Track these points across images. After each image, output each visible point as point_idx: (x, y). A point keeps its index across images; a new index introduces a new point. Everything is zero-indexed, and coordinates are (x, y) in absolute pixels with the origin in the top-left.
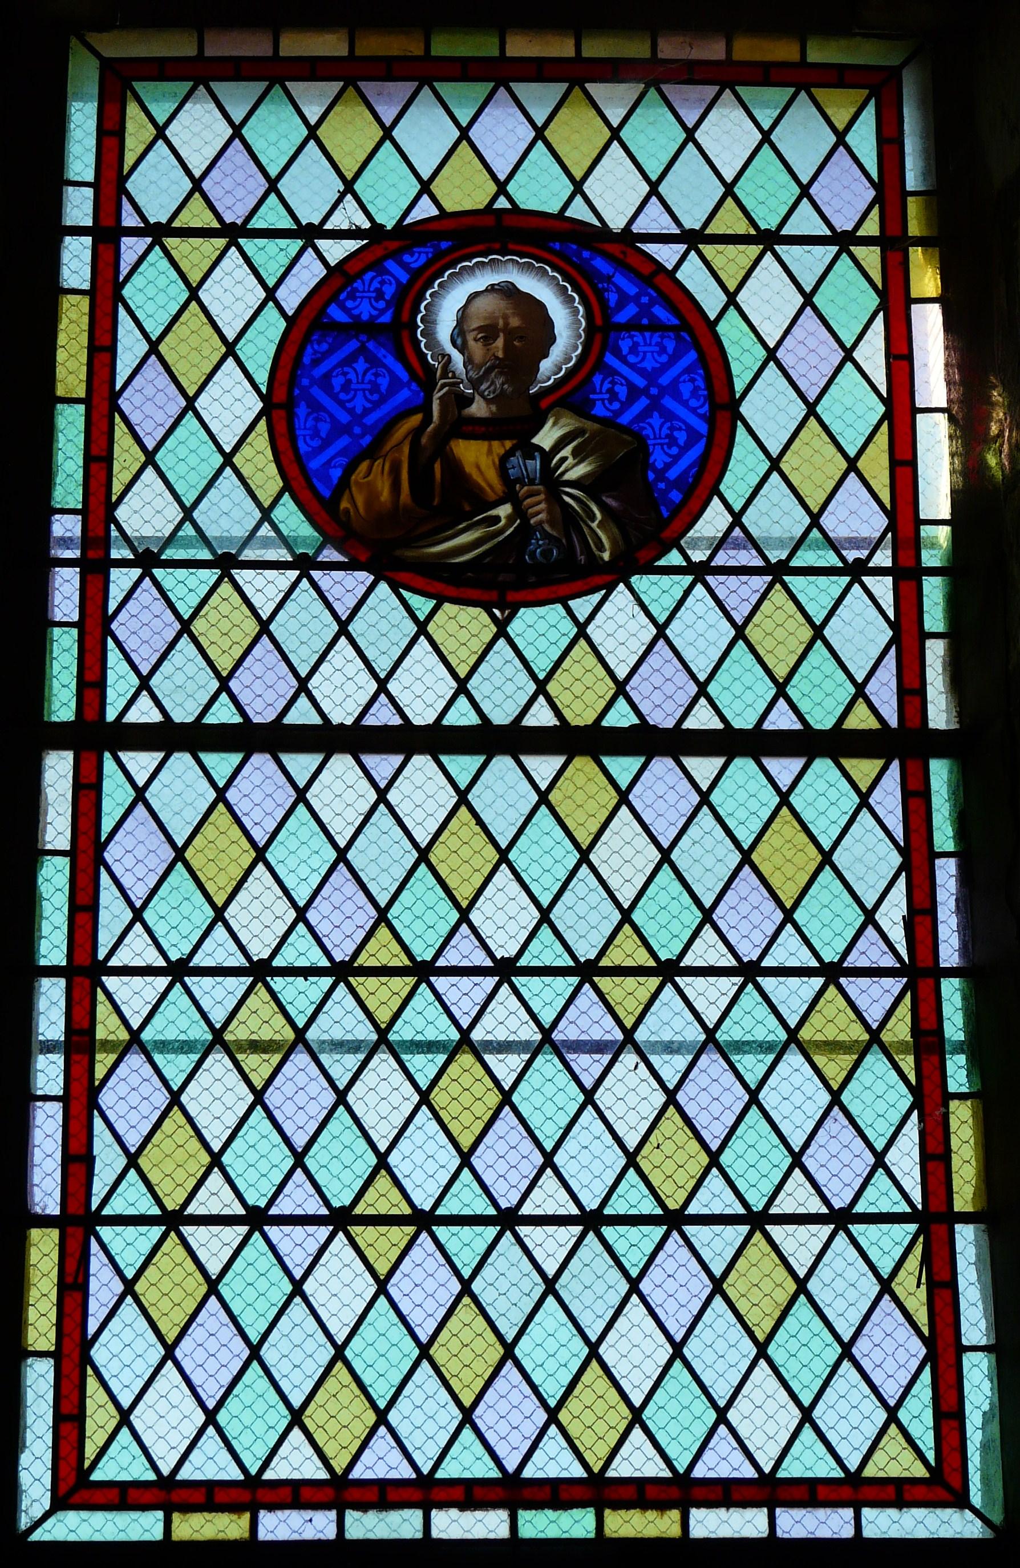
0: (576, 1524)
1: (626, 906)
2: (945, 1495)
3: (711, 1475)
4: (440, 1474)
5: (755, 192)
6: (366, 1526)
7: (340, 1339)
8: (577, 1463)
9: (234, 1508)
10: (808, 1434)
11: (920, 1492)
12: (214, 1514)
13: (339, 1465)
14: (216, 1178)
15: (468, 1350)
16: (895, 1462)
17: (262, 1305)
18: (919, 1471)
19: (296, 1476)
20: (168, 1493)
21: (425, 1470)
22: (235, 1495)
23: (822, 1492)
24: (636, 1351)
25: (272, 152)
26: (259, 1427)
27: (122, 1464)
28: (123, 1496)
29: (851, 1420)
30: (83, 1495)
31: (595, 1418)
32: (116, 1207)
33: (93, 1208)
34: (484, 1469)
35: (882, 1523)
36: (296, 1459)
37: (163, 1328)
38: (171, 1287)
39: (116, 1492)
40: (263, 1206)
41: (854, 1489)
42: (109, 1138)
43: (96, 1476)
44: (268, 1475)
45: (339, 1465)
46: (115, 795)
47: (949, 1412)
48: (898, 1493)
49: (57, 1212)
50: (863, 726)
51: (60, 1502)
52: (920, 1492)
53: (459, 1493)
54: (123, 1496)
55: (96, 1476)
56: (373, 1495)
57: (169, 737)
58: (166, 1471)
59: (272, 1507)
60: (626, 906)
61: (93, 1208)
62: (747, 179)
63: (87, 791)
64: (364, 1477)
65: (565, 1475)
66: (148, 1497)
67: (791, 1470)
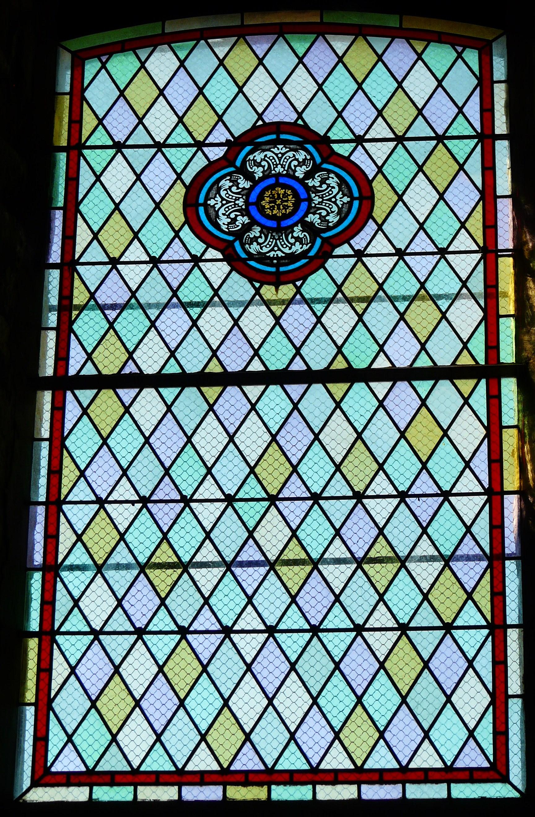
0: (167, 794)
1: (209, 476)
2: (497, 776)
3: (197, 769)
4: (232, 768)
5: (409, 106)
6: (103, 794)
7: (226, 696)
8: (215, 762)
9: (260, 784)
10: (293, 747)
11: (485, 775)
12: (324, 786)
13: (314, 761)
14: (337, 608)
15: (115, 703)
16: (473, 759)
17: (141, 680)
18: (486, 764)
19: (293, 768)
20: (90, 777)
21: (225, 766)
22: (215, 778)
23: (296, 777)
24: (248, 703)
25: (438, 66)
26: (407, 740)
27: (68, 763)
28: (69, 779)
29: (449, 737)
30: (47, 779)
31: (359, 737)
32: (66, 627)
33: (56, 629)
34: (255, 765)
35: (463, 791)
36: (293, 759)
37: (222, 690)
38: (95, 670)
39: (467, 773)
40: (361, 624)
41: (449, 774)
42: (65, 592)
43: (53, 769)
44: (412, 766)
45: (314, 761)
46: (72, 411)
47: (501, 734)
48: (472, 775)
49: (37, 630)
50: (126, 390)
51: (505, 778)
52: (485, 775)
53: (108, 779)
54: (69, 779)
55: (53, 769)
56: (376, 777)
57: (100, 382)
58: (180, 766)
59: (278, 784)
60: (209, 476)
61: (56, 629)
62: (196, 106)
63: (58, 410)
64: (326, 768)
65: (208, 769)
66: (304, 778)
67: (103, 767)
